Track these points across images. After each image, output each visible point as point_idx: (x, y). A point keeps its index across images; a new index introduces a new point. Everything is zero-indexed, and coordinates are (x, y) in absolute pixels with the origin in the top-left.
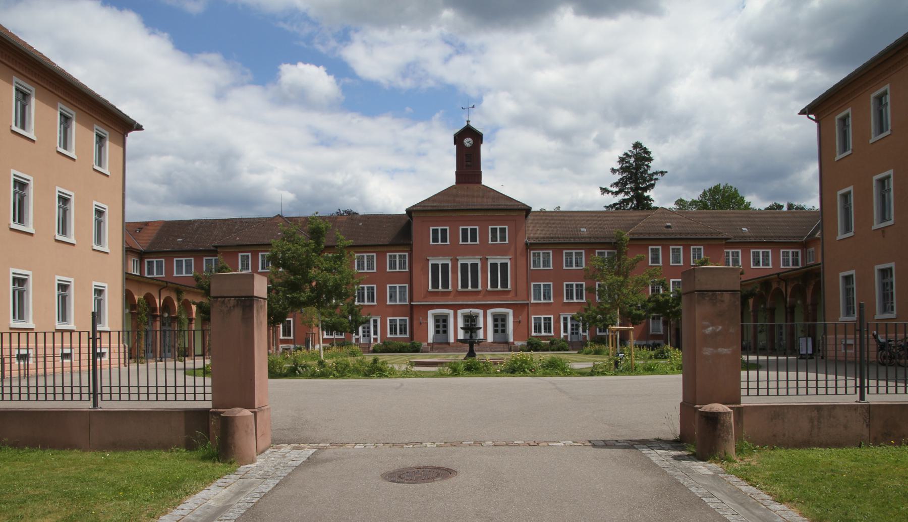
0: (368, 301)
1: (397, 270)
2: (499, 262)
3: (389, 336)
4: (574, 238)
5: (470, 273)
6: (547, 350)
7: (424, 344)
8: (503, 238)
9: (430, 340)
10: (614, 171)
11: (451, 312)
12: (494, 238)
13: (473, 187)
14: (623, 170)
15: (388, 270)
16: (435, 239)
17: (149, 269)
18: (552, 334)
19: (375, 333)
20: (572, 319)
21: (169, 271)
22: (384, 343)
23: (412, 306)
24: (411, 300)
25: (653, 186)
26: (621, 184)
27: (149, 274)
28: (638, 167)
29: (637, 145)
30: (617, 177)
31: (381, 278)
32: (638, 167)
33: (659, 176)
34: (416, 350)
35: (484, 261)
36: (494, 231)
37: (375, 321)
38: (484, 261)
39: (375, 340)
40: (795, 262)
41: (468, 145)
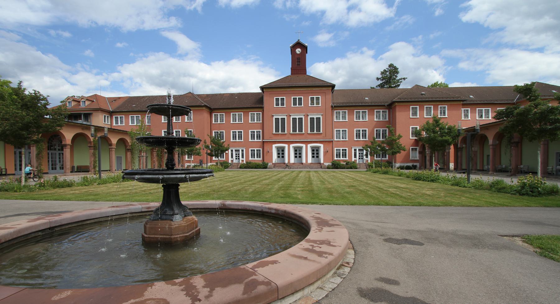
0: (239, 139)
1: (256, 122)
3: (250, 159)
4: (362, 103)
5: (298, 124)
6: (344, 168)
8: (318, 103)
10: (378, 79)
11: (286, 146)
13: (301, 76)
14: (383, 79)
15: (250, 122)
17: (116, 121)
18: (347, 159)
19: (243, 157)
20: (359, 150)
21: (127, 122)
22: (247, 162)
24: (263, 139)
27: (116, 124)
28: (391, 77)
29: (391, 66)
30: (380, 82)
31: (247, 126)
32: (391, 77)
33: (403, 80)
34: (265, 166)
37: (243, 151)
39: (243, 161)
41: (299, 55)
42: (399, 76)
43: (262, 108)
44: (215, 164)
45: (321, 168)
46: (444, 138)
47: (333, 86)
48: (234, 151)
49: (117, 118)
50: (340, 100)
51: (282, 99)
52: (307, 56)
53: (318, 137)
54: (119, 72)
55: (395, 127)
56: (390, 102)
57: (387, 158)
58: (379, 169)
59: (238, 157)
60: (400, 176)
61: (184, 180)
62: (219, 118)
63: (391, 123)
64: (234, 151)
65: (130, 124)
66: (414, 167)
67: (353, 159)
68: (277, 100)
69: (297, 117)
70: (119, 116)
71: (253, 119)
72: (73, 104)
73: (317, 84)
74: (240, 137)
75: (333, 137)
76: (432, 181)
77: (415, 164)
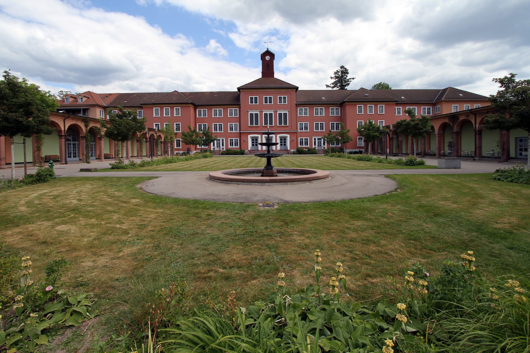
2: (283, 113)
3: (229, 147)
5: (268, 118)
6: (307, 154)
7: (246, 151)
8: (285, 102)
9: (249, 149)
11: (259, 136)
12: (280, 102)
16: (252, 102)
19: (223, 145)
23: (240, 133)
24: (240, 130)
25: (349, 84)
26: (335, 84)
28: (342, 76)
29: (342, 67)
30: (333, 81)
31: (226, 120)
32: (342, 76)
33: (352, 80)
34: (242, 153)
35: (276, 112)
36: (280, 98)
37: (223, 140)
38: (276, 112)
39: (223, 149)
40: (429, 113)
42: (349, 76)
43: (239, 105)
44: (199, 151)
45: (288, 153)
46: (375, 134)
47: (297, 88)
50: (303, 99)
52: (275, 61)
53: (286, 129)
55: (345, 123)
56: (341, 102)
57: (340, 145)
58: (334, 154)
59: (218, 146)
60: (349, 158)
61: (272, 157)
62: (202, 113)
63: (342, 119)
66: (361, 152)
67: (314, 146)
68: (252, 98)
69: (268, 113)
71: (231, 114)
72: (71, 100)
73: (284, 86)
74: (220, 129)
75: (297, 129)
76: (368, 161)
77: (361, 150)
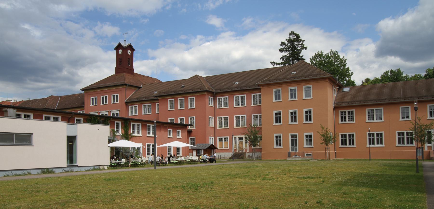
17: (144, 110)
48: (237, 139)
49: (220, 100)
51: (117, 96)
54: (153, 58)
64: (237, 139)
65: (143, 114)
70: (223, 98)
